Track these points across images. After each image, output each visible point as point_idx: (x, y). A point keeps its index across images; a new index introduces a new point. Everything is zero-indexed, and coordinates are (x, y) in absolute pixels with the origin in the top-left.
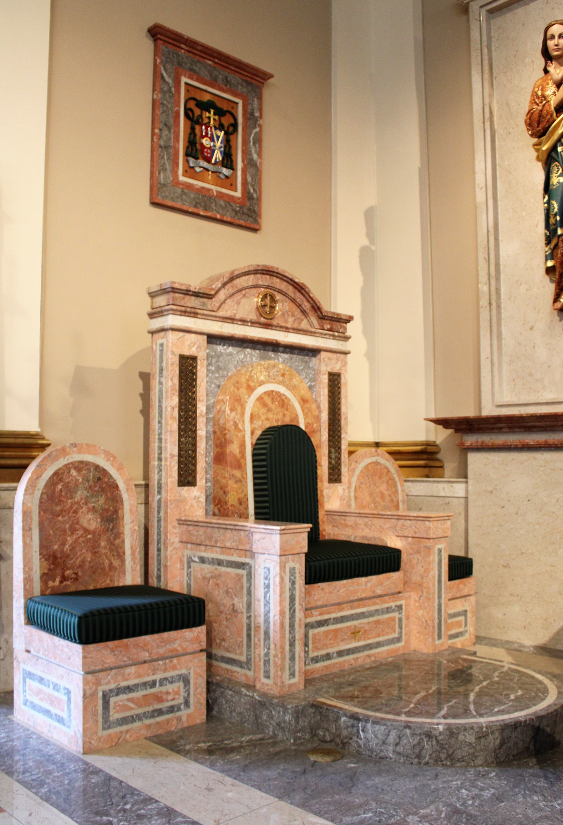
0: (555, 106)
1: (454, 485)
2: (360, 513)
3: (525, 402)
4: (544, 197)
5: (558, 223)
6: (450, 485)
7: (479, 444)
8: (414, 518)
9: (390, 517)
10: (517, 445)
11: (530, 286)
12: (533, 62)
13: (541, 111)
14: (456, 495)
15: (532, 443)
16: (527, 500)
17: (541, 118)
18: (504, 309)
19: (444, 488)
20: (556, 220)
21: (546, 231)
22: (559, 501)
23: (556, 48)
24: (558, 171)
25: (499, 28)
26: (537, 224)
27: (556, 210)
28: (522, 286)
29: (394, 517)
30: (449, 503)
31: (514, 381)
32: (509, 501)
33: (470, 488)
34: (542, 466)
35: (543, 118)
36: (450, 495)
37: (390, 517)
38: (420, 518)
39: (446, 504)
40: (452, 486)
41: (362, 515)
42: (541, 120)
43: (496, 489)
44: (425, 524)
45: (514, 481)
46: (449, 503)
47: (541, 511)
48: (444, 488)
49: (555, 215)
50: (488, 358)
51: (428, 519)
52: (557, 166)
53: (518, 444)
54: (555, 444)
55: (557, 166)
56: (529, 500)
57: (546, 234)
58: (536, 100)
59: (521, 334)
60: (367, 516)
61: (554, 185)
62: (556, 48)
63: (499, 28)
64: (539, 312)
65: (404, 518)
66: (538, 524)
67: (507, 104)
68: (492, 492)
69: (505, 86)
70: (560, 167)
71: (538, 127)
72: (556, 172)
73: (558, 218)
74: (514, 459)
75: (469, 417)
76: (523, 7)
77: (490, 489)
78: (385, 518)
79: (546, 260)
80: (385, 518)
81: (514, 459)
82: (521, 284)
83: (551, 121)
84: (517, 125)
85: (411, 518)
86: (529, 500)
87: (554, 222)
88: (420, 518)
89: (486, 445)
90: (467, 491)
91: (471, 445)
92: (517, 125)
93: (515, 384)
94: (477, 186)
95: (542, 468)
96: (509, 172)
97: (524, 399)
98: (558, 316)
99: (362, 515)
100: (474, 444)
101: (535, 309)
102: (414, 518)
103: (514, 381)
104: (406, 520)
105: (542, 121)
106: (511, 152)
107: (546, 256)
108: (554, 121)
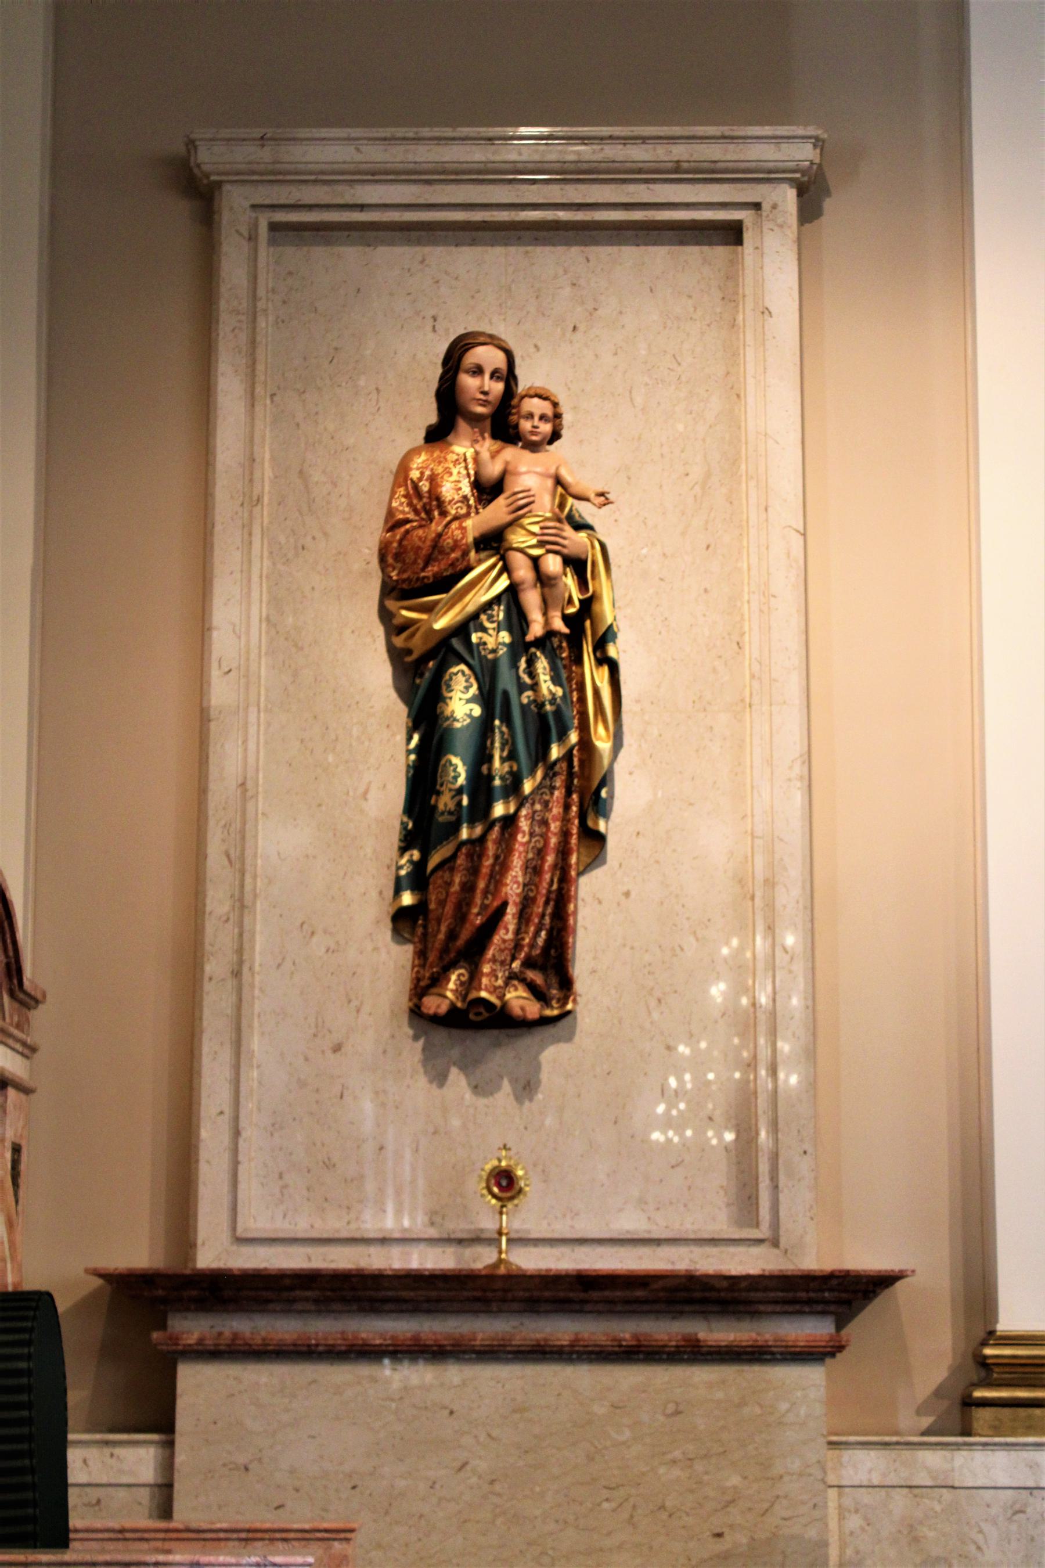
0: (477, 534)
1: (118, 1451)
2: (122, 1531)
3: (325, 1236)
4: (409, 739)
5: (465, 812)
6: (107, 1451)
7: (224, 1341)
8: (299, 1535)
9: (222, 1535)
10: (333, 1345)
11: (337, 943)
12: (377, 389)
13: (439, 535)
14: (125, 1480)
15: (378, 1342)
16: (350, 1485)
17: (436, 552)
18: (261, 990)
19: (85, 1461)
20: (459, 804)
21: (405, 819)
22: (437, 1486)
23: (482, 397)
24: (467, 688)
25: (290, 273)
26: (366, 792)
27: (461, 780)
28: (315, 939)
29: (235, 1536)
30: (99, 1502)
31: (281, 1177)
32: (297, 1490)
33: (180, 1458)
34: (392, 1400)
35: (442, 552)
36: (104, 1480)
37: (222, 1535)
38: (319, 1535)
39: (89, 1505)
40: (112, 1455)
41: (128, 1535)
42: (434, 556)
43: (260, 1460)
44: (330, 1548)
45: (314, 1437)
46: (99, 1502)
47: (387, 1513)
48: (85, 1461)
49: (460, 791)
50: (222, 1113)
51: (342, 1535)
52: (463, 672)
53: (339, 1342)
54: (440, 1346)
55: (463, 672)
56: (354, 1487)
57: (404, 826)
58: (415, 501)
59: (306, 1059)
60: (146, 1535)
61: (455, 720)
62: (482, 397)
63: (290, 273)
64: (358, 1011)
65: (267, 1536)
66: (379, 1546)
67: (301, 472)
68: (247, 1469)
69: (298, 425)
70: (472, 680)
71: (423, 569)
72: (461, 688)
73: (465, 801)
74: (314, 1381)
75: (230, 1270)
76: (360, 248)
77: (242, 1459)
78: (204, 1540)
79: (398, 892)
80: (204, 1540)
81: (314, 1381)
82: (313, 933)
83: (460, 566)
84: (326, 534)
85: (292, 1535)
86: (354, 1487)
87: (451, 806)
88: (319, 1535)
89: (247, 1344)
90: (168, 1466)
91: (201, 1341)
92: (326, 534)
93: (286, 1186)
94: (214, 665)
95: (394, 1405)
96: (296, 645)
97: (302, 1225)
98: (411, 1025)
99: (128, 1535)
100: (207, 1342)
101: (350, 1001)
102: (299, 1535)
103: (281, 1177)
104: (272, 1540)
105: (436, 560)
106: (304, 597)
107: (398, 880)
108: (469, 569)
